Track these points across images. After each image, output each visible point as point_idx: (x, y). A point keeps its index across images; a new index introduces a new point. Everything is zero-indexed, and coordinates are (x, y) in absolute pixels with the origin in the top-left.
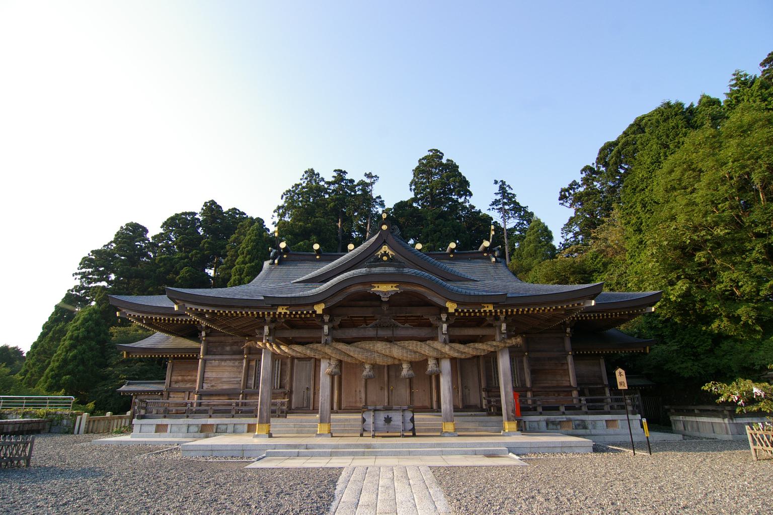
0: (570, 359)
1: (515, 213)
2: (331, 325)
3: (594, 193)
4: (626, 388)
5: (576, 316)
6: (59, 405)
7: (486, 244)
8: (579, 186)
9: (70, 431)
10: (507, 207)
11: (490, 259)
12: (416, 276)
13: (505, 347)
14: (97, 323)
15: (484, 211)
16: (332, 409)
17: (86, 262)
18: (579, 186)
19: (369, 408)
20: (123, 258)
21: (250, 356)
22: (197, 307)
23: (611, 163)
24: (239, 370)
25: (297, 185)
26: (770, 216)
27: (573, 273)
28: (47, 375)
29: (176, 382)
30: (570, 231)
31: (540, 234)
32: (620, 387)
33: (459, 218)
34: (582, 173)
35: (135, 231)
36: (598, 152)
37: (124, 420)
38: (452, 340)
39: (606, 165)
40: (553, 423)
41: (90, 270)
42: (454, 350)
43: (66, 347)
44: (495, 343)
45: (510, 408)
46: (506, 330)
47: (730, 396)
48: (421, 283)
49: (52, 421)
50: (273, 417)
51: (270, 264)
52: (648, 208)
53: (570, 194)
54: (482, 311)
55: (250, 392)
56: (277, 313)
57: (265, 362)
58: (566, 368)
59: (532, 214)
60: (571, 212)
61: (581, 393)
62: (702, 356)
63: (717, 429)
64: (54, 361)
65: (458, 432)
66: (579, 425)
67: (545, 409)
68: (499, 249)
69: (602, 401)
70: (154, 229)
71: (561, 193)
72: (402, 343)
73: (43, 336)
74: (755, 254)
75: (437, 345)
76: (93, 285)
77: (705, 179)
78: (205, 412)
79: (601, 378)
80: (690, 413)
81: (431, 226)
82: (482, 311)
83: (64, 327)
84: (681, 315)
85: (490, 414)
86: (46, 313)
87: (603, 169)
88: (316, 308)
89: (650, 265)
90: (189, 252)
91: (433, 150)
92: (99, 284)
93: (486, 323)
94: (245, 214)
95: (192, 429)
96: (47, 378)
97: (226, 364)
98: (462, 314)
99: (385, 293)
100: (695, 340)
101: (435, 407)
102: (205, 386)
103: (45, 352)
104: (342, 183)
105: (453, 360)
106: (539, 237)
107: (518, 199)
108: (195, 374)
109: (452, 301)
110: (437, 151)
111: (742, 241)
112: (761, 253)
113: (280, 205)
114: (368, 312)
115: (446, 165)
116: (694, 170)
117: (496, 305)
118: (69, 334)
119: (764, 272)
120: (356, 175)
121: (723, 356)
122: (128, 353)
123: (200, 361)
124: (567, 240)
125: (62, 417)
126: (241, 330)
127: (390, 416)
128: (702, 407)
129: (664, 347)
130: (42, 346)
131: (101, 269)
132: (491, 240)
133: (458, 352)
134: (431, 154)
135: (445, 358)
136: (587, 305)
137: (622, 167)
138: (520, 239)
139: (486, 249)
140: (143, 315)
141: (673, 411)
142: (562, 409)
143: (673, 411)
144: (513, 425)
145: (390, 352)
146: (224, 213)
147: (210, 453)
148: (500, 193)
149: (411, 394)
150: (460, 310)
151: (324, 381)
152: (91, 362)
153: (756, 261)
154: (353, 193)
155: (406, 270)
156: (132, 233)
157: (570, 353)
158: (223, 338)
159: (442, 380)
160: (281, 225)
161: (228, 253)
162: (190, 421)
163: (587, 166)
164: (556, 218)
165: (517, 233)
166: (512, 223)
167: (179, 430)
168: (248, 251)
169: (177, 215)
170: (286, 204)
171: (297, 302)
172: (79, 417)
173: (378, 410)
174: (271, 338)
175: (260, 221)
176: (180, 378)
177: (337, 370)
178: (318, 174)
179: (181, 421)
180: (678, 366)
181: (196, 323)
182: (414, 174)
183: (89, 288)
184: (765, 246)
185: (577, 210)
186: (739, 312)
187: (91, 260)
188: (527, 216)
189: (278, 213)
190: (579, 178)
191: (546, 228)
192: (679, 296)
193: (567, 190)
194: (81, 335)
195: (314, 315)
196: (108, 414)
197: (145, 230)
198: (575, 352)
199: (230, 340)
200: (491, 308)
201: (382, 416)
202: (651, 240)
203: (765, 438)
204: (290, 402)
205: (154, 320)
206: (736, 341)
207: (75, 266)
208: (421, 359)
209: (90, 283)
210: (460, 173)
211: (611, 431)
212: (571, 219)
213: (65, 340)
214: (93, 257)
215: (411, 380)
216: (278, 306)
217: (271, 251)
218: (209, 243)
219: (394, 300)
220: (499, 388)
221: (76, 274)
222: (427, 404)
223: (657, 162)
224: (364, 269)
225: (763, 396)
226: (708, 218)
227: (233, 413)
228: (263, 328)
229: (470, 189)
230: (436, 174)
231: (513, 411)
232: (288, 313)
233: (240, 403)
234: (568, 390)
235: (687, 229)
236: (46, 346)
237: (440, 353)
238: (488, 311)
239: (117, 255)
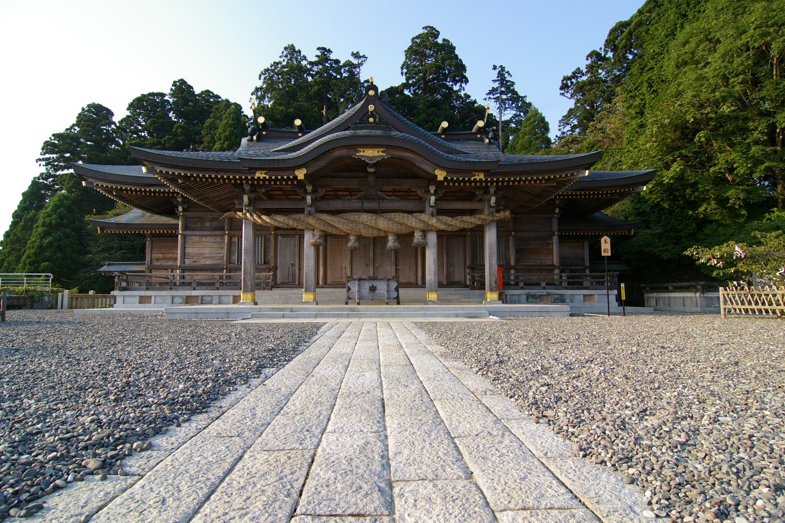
0: (555, 239)
1: (513, 103)
2: (314, 196)
3: (598, 82)
4: (609, 254)
6: (43, 284)
8: (583, 74)
9: (53, 306)
10: (504, 97)
11: (482, 140)
12: (404, 140)
13: (493, 220)
14: (70, 210)
15: (481, 102)
16: (318, 284)
17: (48, 147)
18: (583, 74)
19: (355, 277)
20: (89, 143)
21: (232, 232)
22: (167, 170)
23: (620, 46)
24: (221, 246)
25: (276, 64)
26: (781, 92)
28: (24, 262)
29: (157, 260)
30: (568, 124)
31: (537, 125)
32: (603, 254)
33: (453, 108)
34: (587, 59)
35: (95, 116)
36: (607, 33)
37: (108, 299)
38: (440, 212)
39: (615, 49)
40: (533, 296)
41: (55, 156)
42: (442, 222)
43: (39, 234)
44: (483, 217)
45: (493, 280)
46: (496, 203)
47: (710, 259)
48: (409, 147)
49: (32, 297)
50: (258, 289)
51: (248, 141)
52: (654, 88)
53: (572, 83)
57: (246, 232)
58: (551, 247)
59: (530, 104)
60: (571, 104)
61: (562, 271)
62: (684, 240)
63: (687, 303)
64: (29, 248)
65: (441, 301)
66: (557, 299)
68: (493, 130)
70: (120, 113)
71: (563, 81)
72: (389, 215)
73: (14, 225)
74: (756, 135)
75: (424, 217)
76: (60, 173)
77: (721, 49)
78: (189, 284)
79: (583, 260)
80: (666, 290)
81: (423, 116)
82: (472, 179)
83: (35, 215)
84: (670, 200)
85: (473, 288)
86: (14, 202)
87: (610, 55)
88: (297, 173)
89: (648, 145)
90: (161, 138)
91: (428, 27)
92: (66, 172)
94: (220, 98)
95: (176, 300)
96: (25, 264)
97: (207, 240)
100: (679, 224)
101: (420, 283)
102: (187, 262)
103: (18, 241)
104: (327, 64)
105: (441, 234)
106: (534, 129)
107: (516, 88)
108: (175, 251)
109: (442, 168)
110: (432, 28)
111: (746, 119)
112: (762, 133)
113: (258, 87)
115: (442, 45)
116: (710, 41)
117: (487, 173)
118: (40, 221)
119: (762, 154)
120: (341, 55)
121: (705, 239)
122: (102, 229)
123: (179, 236)
124: (563, 133)
125: (42, 294)
128: (675, 284)
129: (649, 231)
130: (15, 235)
131: (68, 155)
133: (445, 224)
134: (426, 31)
135: (431, 230)
136: (581, 175)
137: (631, 53)
138: (514, 132)
139: (479, 128)
140: (112, 185)
141: (648, 289)
143: (648, 289)
144: (495, 296)
145: (376, 223)
146: (197, 95)
147: (195, 315)
148: (498, 80)
149: (397, 270)
151: (309, 252)
152: (69, 250)
153: (756, 143)
154: (338, 77)
155: (394, 133)
158: (201, 214)
159: (428, 252)
161: (204, 139)
162: (174, 293)
163: (594, 51)
164: (556, 110)
165: (513, 125)
166: (508, 115)
167: (164, 301)
168: (226, 137)
169: (143, 96)
170: (265, 86)
171: (277, 165)
172: (60, 294)
173: (363, 280)
174: (251, 208)
175: (238, 107)
176: (160, 256)
177: (321, 241)
178: (299, 52)
179: (164, 293)
180: (659, 249)
182: (406, 55)
183: (56, 176)
184: (768, 127)
185: (578, 101)
186: (729, 193)
187: (53, 145)
188: (523, 106)
189: (257, 95)
190: (583, 64)
191: (543, 119)
192: (672, 178)
193: (569, 78)
194: (54, 222)
196: (91, 292)
199: (209, 215)
200: (481, 176)
201: (367, 285)
202: (653, 119)
203: (737, 297)
204: (275, 276)
206: (719, 225)
207: (37, 152)
208: (407, 232)
209: (56, 170)
210: (457, 56)
211: (587, 304)
212: (571, 110)
213: (37, 227)
214: (56, 142)
215: (396, 251)
216: (257, 169)
217: (249, 127)
218: (183, 128)
220: (484, 266)
221: (40, 160)
222: (412, 280)
223: (672, 34)
225: (743, 257)
226: (717, 93)
227: (217, 285)
229: (467, 74)
230: (430, 56)
231: (496, 282)
232: (267, 177)
233: (224, 277)
234: (551, 268)
235: (693, 106)
236: (19, 234)
237: (427, 224)
239: (82, 140)
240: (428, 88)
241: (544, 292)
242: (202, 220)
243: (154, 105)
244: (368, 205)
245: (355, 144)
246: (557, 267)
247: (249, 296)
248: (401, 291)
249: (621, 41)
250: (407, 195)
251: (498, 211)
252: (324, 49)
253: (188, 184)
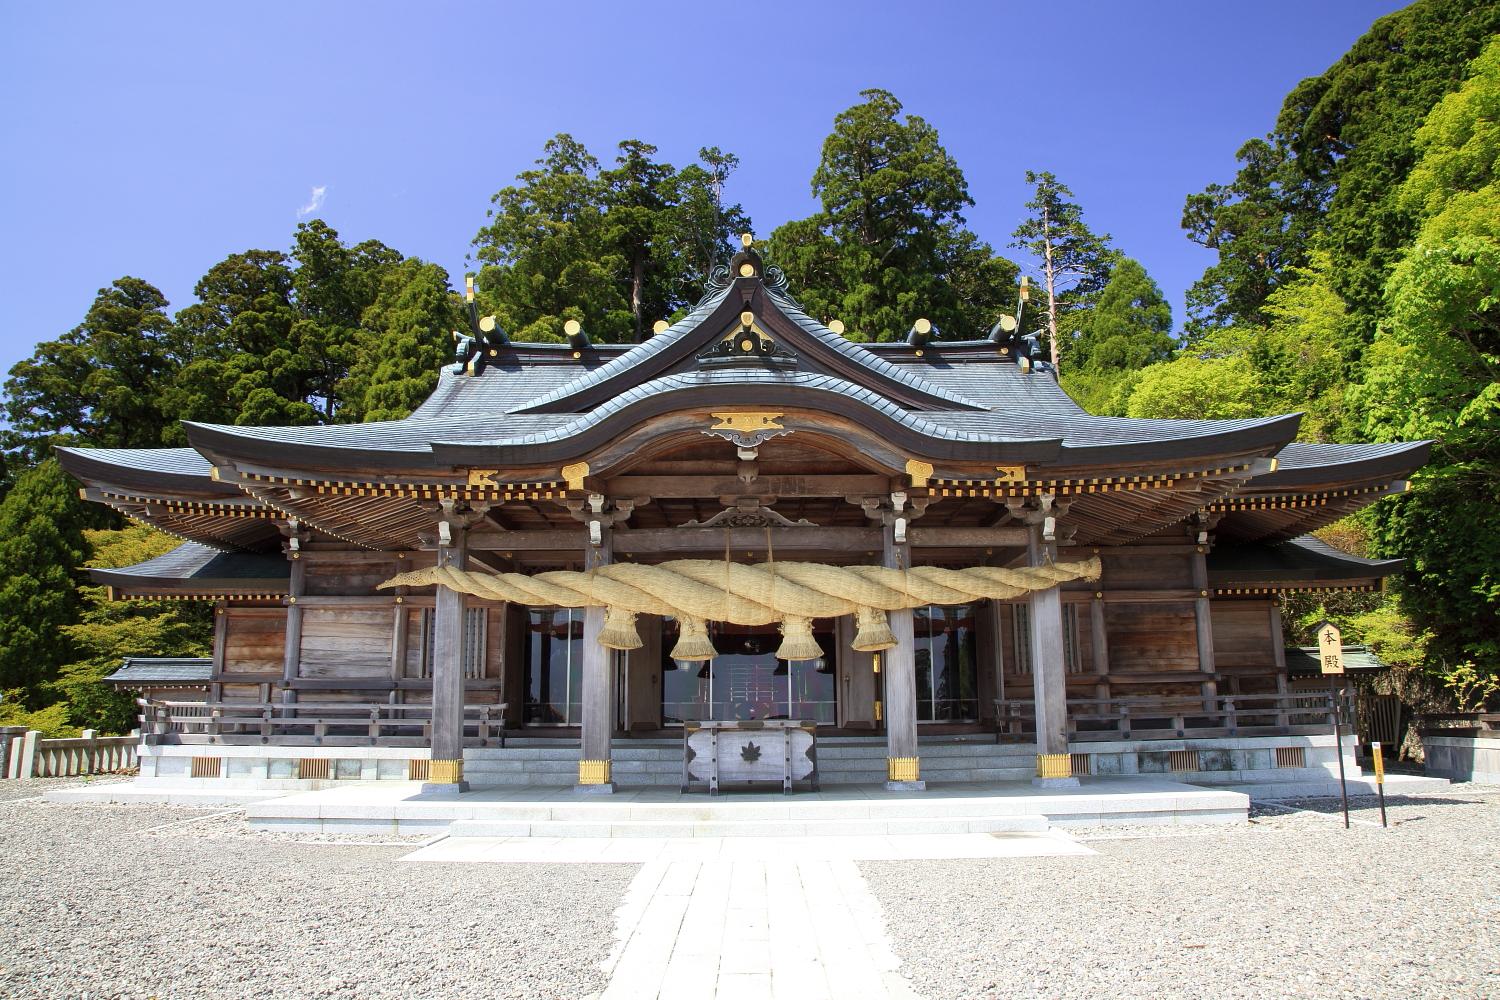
0: (1204, 606)
5: (1226, 501)
15: (1002, 252)
29: (239, 660)
35: (129, 305)
38: (919, 557)
40: (1155, 757)
46: (1056, 533)
54: (998, 484)
55: (412, 686)
56: (469, 488)
57: (448, 617)
60: (1212, 259)
61: (1223, 688)
66: (1214, 761)
67: (1137, 724)
69: (1271, 704)
70: (180, 298)
93: (1004, 519)
97: (351, 620)
98: (946, 493)
99: (747, 437)
114: (704, 488)
120: (675, 153)
126: (383, 535)
127: (755, 745)
132: (1019, 315)
136: (1258, 471)
142: (1179, 724)
150: (941, 482)
156: (129, 305)
157: (1204, 593)
160: (492, 282)
172: (17, 741)
175: (440, 278)
181: (273, 516)
195: (563, 494)
197: (159, 299)
198: (1216, 591)
205: (171, 509)
211: (1288, 772)
217: (459, 340)
224: (692, 375)
228: (435, 530)
232: (496, 487)
234: (1191, 684)
238: (1012, 484)
241: (1180, 745)
246: (1211, 677)
250: (838, 513)
252: (635, 144)
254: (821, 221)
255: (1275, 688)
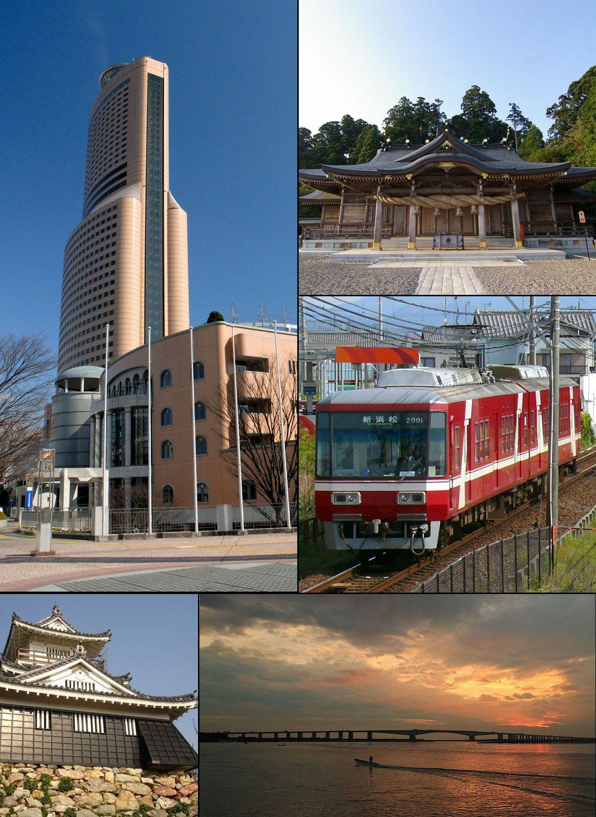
0: (552, 205)
7: (505, 140)
11: (506, 148)
12: (465, 158)
15: (504, 121)
25: (396, 106)
27: (555, 156)
39: (573, 94)
40: (543, 242)
55: (369, 224)
57: (378, 207)
60: (553, 122)
61: (559, 225)
65: (488, 247)
75: (477, 197)
78: (344, 236)
85: (507, 237)
105: (486, 206)
107: (523, 114)
114: (437, 179)
120: (430, 100)
142: (548, 234)
144: (520, 243)
151: (412, 218)
160: (387, 129)
162: (336, 241)
164: (545, 125)
166: (519, 128)
175: (375, 127)
179: (330, 241)
188: (528, 124)
190: (558, 102)
197: (310, 132)
199: (358, 194)
200: (507, 176)
201: (445, 238)
211: (576, 246)
219: (452, 172)
222: (471, 231)
234: (551, 223)
237: (478, 202)
240: (475, 115)
241: (549, 239)
242: (354, 197)
243: (332, 127)
244: (445, 191)
245: (438, 160)
247: (378, 244)
248: (465, 238)
249: (576, 91)
250: (468, 185)
251: (518, 193)
253: (349, 182)
254: (463, 115)
255: (572, 225)
